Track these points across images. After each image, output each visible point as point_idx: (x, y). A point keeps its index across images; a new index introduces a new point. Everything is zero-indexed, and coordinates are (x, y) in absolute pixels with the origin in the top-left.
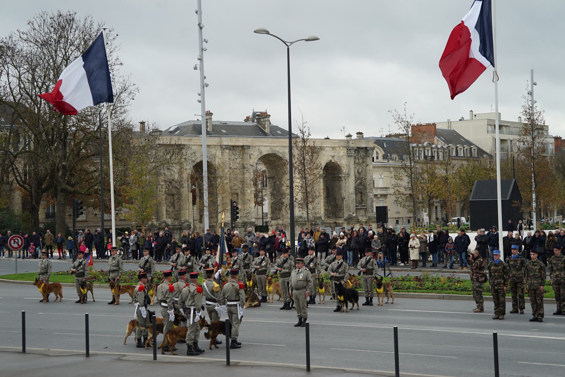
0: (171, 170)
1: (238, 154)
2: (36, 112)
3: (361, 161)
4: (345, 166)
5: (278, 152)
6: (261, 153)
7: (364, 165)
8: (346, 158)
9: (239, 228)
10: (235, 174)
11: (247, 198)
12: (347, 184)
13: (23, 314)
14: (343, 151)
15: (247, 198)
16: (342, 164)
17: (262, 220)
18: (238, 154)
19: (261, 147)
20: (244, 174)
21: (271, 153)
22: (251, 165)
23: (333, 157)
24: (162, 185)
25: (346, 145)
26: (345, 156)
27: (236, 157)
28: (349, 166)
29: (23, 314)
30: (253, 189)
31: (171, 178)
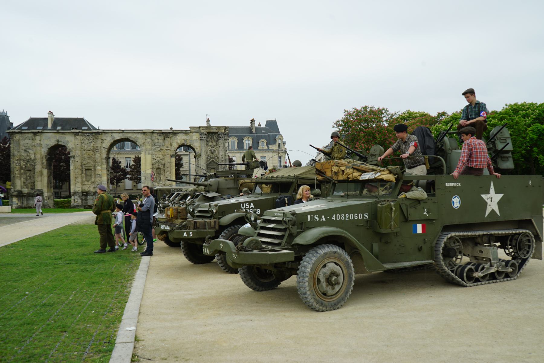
0: (28, 152)
1: (92, 139)
2: (447, 185)
3: (214, 144)
4: (198, 148)
5: (130, 137)
6: (114, 138)
7: (218, 146)
8: (199, 141)
9: (92, 196)
10: (89, 155)
11: (97, 173)
12: (200, 162)
13: (311, 145)
14: (196, 136)
15: (97, 173)
16: (195, 146)
17: (189, 174)
18: (92, 139)
19: (114, 134)
21: (123, 138)
22: (104, 147)
24: (16, 163)
25: (199, 131)
26: (198, 140)
27: (90, 141)
28: (201, 147)
29: (311, 145)
30: (106, 166)
31: (28, 158)
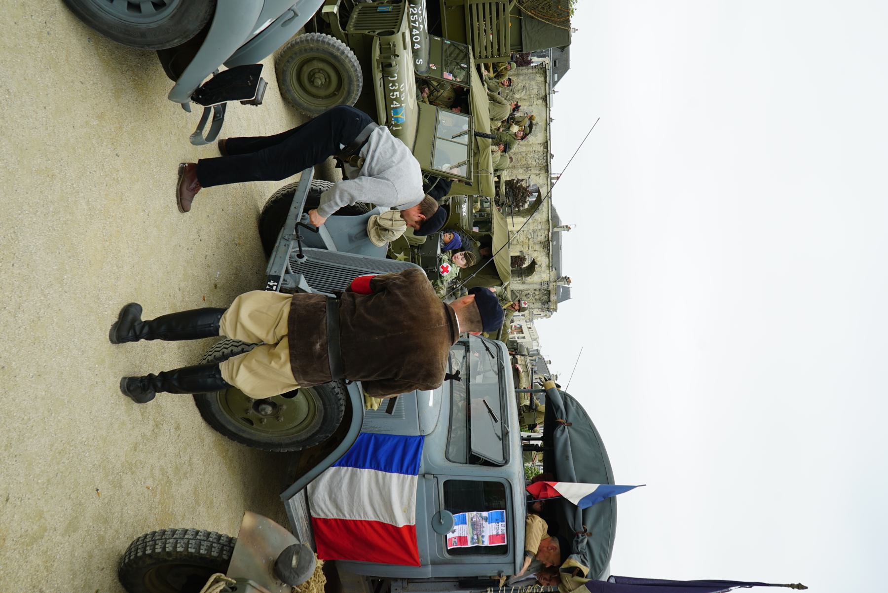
5: (543, 205)
18: (540, 163)
20: (521, 168)
23: (540, 266)
27: (537, 160)
